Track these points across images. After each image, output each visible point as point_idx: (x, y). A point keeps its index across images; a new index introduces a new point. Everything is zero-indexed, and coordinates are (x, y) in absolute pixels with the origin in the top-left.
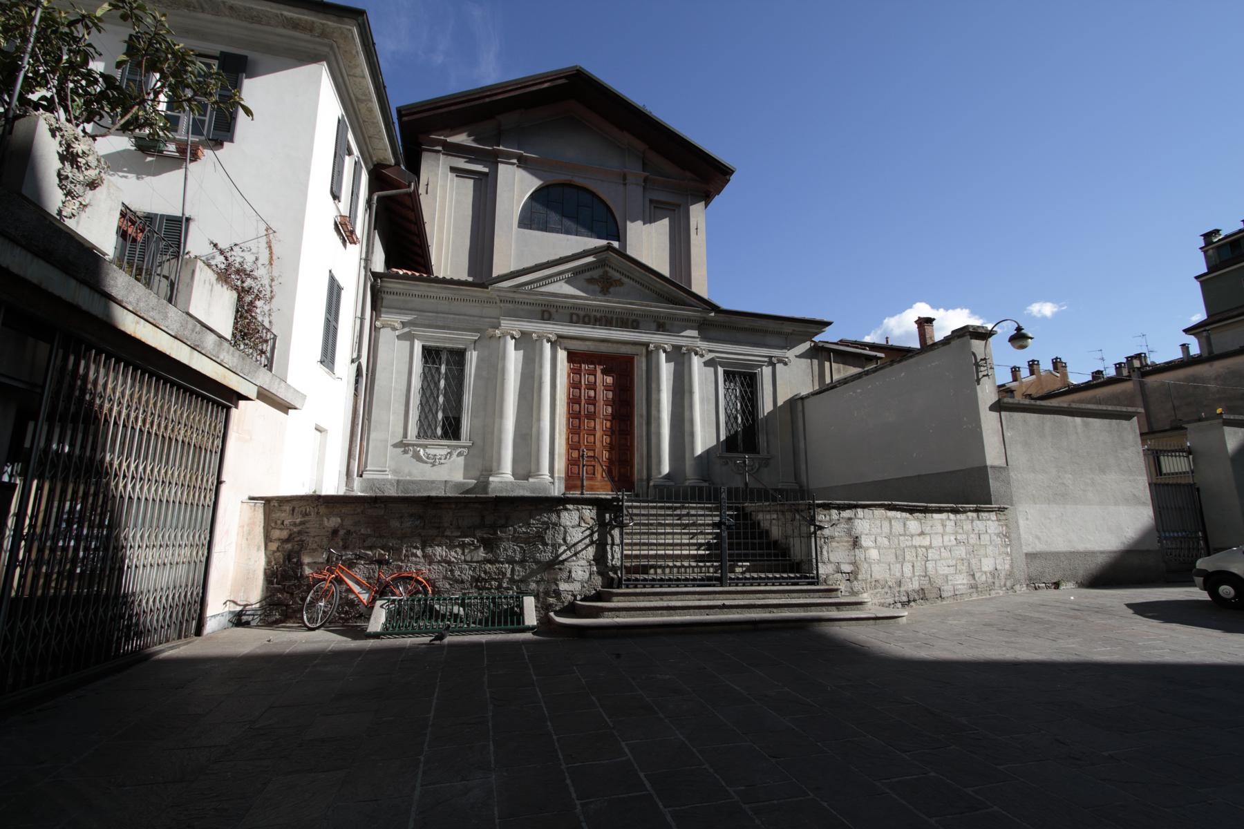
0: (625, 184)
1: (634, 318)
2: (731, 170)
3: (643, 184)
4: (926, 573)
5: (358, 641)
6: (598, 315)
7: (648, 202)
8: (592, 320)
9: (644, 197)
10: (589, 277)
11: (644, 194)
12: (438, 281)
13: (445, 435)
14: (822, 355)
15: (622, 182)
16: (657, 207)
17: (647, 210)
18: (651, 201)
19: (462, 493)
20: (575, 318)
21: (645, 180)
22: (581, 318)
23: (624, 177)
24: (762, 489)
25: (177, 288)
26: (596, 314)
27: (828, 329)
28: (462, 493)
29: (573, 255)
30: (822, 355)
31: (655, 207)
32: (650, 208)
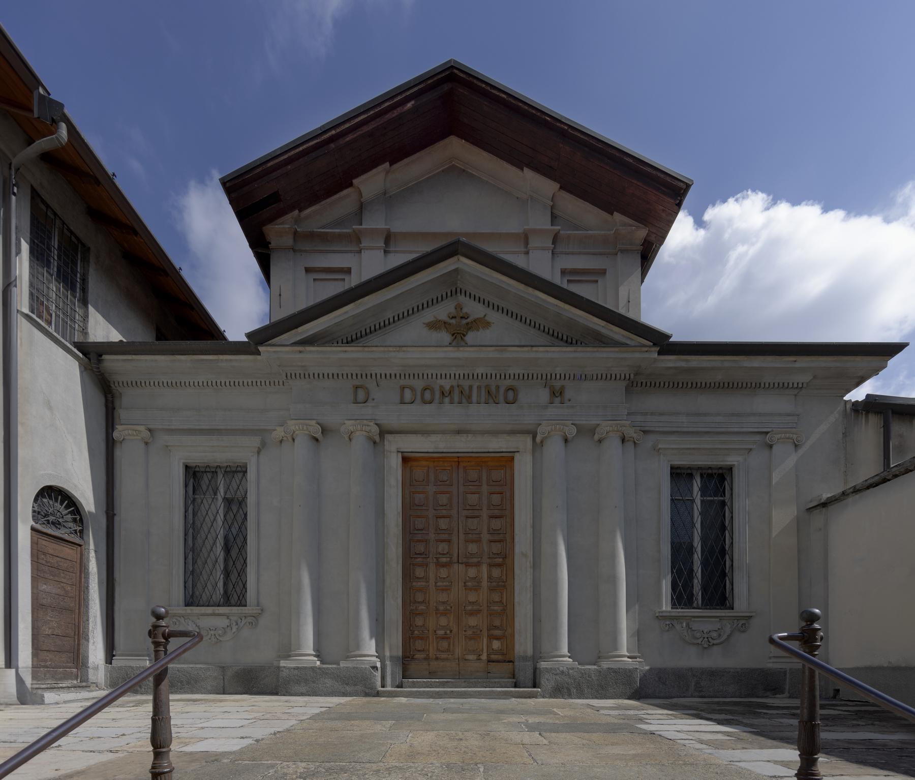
0: (527, 253)
1: (508, 382)
2: (686, 184)
6: (447, 384)
8: (437, 395)
9: (552, 267)
10: (432, 319)
12: (237, 348)
13: (227, 601)
15: (523, 249)
19: (839, 669)
20: (408, 394)
21: (555, 239)
22: (419, 394)
25: (859, 725)
26: (442, 382)
27: (893, 362)
28: (839, 669)
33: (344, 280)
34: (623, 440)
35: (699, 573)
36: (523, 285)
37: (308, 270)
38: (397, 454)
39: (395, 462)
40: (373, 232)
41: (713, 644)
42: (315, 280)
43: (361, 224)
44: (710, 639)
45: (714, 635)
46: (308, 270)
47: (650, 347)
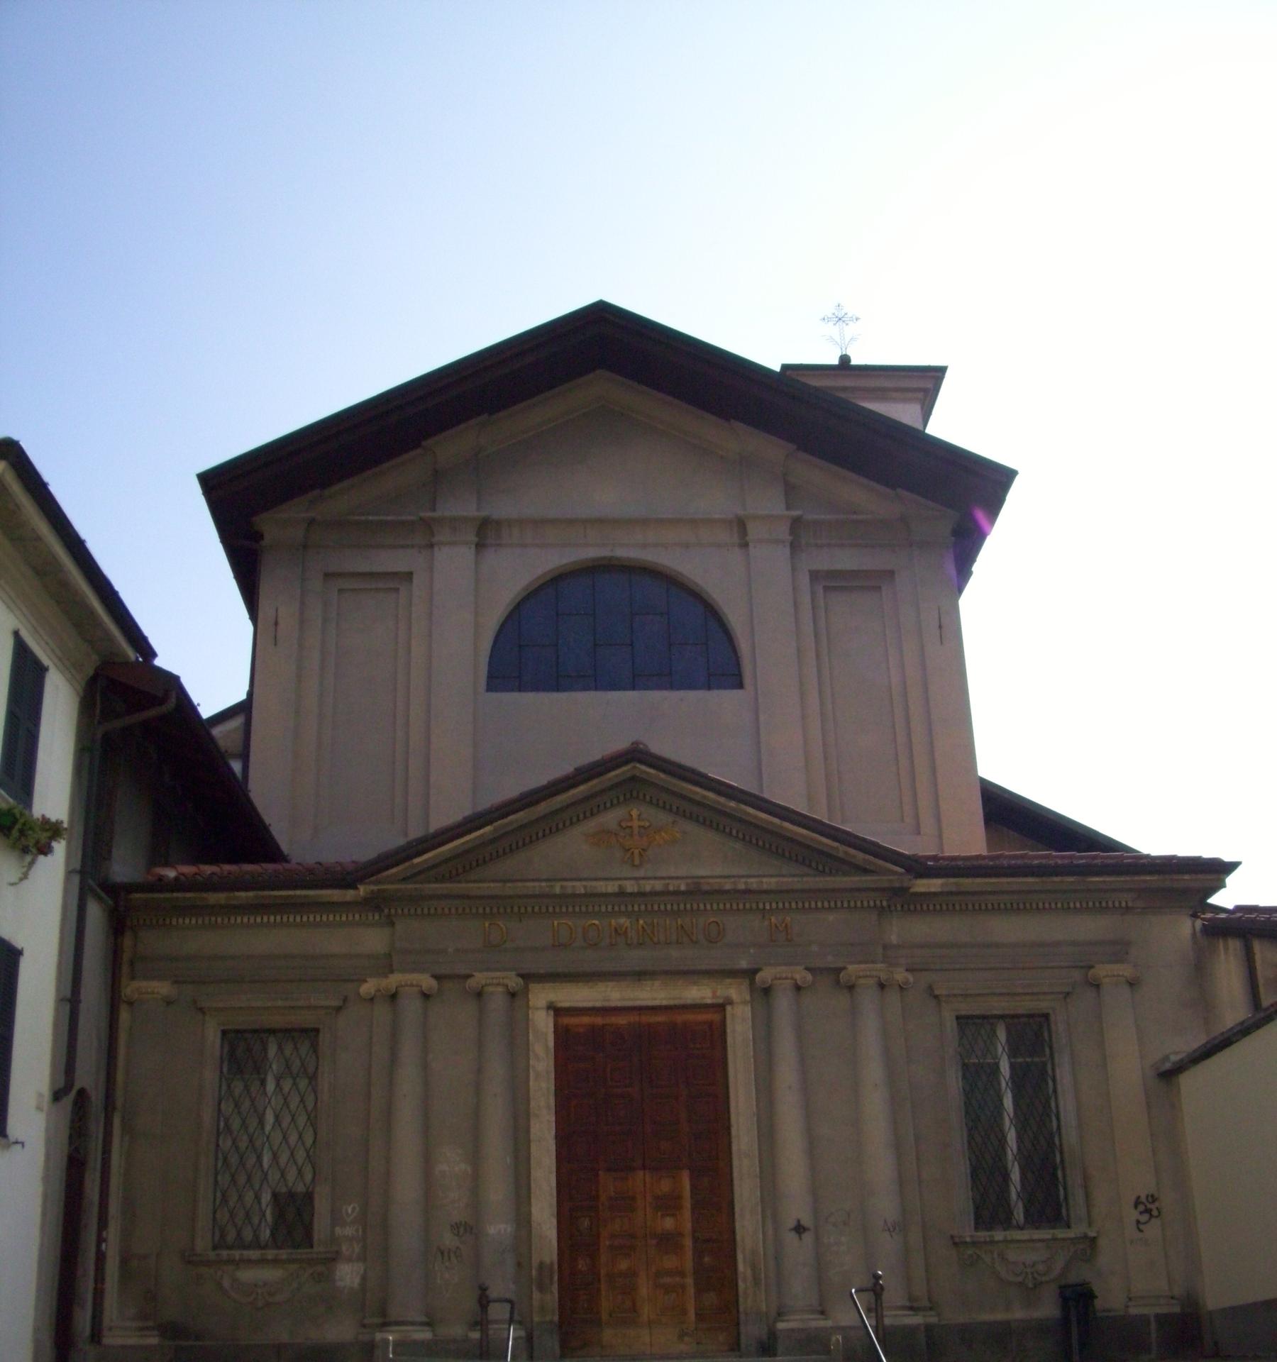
0: (745, 545)
3: (790, 538)
4: (20, 838)
5: (110, 1201)
7: (805, 581)
9: (794, 569)
11: (792, 558)
14: (1226, 949)
16: (835, 589)
17: (806, 599)
18: (815, 576)
21: (796, 524)
23: (741, 525)
24: (919, 1325)
29: (578, 771)
30: (1226, 949)
31: (826, 589)
32: (813, 593)
33: (397, 590)
34: (882, 986)
35: (1015, 1175)
36: (689, 1002)
37: (328, 576)
38: (547, 1012)
39: (543, 1023)
40: (455, 523)
41: (1042, 1283)
42: (340, 591)
43: (434, 510)
44: (1036, 1275)
45: (1041, 1267)
46: (328, 576)
47: (901, 874)
